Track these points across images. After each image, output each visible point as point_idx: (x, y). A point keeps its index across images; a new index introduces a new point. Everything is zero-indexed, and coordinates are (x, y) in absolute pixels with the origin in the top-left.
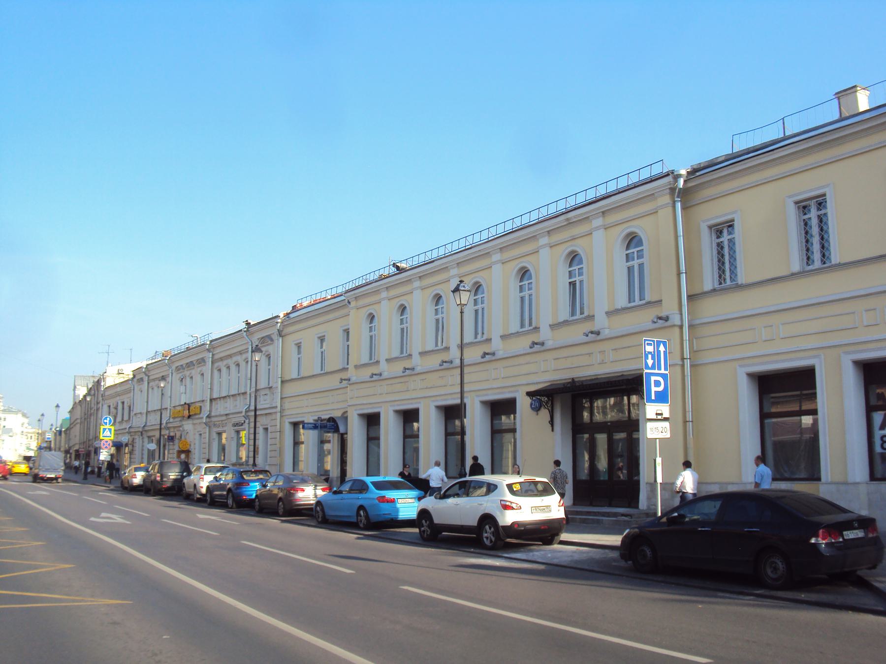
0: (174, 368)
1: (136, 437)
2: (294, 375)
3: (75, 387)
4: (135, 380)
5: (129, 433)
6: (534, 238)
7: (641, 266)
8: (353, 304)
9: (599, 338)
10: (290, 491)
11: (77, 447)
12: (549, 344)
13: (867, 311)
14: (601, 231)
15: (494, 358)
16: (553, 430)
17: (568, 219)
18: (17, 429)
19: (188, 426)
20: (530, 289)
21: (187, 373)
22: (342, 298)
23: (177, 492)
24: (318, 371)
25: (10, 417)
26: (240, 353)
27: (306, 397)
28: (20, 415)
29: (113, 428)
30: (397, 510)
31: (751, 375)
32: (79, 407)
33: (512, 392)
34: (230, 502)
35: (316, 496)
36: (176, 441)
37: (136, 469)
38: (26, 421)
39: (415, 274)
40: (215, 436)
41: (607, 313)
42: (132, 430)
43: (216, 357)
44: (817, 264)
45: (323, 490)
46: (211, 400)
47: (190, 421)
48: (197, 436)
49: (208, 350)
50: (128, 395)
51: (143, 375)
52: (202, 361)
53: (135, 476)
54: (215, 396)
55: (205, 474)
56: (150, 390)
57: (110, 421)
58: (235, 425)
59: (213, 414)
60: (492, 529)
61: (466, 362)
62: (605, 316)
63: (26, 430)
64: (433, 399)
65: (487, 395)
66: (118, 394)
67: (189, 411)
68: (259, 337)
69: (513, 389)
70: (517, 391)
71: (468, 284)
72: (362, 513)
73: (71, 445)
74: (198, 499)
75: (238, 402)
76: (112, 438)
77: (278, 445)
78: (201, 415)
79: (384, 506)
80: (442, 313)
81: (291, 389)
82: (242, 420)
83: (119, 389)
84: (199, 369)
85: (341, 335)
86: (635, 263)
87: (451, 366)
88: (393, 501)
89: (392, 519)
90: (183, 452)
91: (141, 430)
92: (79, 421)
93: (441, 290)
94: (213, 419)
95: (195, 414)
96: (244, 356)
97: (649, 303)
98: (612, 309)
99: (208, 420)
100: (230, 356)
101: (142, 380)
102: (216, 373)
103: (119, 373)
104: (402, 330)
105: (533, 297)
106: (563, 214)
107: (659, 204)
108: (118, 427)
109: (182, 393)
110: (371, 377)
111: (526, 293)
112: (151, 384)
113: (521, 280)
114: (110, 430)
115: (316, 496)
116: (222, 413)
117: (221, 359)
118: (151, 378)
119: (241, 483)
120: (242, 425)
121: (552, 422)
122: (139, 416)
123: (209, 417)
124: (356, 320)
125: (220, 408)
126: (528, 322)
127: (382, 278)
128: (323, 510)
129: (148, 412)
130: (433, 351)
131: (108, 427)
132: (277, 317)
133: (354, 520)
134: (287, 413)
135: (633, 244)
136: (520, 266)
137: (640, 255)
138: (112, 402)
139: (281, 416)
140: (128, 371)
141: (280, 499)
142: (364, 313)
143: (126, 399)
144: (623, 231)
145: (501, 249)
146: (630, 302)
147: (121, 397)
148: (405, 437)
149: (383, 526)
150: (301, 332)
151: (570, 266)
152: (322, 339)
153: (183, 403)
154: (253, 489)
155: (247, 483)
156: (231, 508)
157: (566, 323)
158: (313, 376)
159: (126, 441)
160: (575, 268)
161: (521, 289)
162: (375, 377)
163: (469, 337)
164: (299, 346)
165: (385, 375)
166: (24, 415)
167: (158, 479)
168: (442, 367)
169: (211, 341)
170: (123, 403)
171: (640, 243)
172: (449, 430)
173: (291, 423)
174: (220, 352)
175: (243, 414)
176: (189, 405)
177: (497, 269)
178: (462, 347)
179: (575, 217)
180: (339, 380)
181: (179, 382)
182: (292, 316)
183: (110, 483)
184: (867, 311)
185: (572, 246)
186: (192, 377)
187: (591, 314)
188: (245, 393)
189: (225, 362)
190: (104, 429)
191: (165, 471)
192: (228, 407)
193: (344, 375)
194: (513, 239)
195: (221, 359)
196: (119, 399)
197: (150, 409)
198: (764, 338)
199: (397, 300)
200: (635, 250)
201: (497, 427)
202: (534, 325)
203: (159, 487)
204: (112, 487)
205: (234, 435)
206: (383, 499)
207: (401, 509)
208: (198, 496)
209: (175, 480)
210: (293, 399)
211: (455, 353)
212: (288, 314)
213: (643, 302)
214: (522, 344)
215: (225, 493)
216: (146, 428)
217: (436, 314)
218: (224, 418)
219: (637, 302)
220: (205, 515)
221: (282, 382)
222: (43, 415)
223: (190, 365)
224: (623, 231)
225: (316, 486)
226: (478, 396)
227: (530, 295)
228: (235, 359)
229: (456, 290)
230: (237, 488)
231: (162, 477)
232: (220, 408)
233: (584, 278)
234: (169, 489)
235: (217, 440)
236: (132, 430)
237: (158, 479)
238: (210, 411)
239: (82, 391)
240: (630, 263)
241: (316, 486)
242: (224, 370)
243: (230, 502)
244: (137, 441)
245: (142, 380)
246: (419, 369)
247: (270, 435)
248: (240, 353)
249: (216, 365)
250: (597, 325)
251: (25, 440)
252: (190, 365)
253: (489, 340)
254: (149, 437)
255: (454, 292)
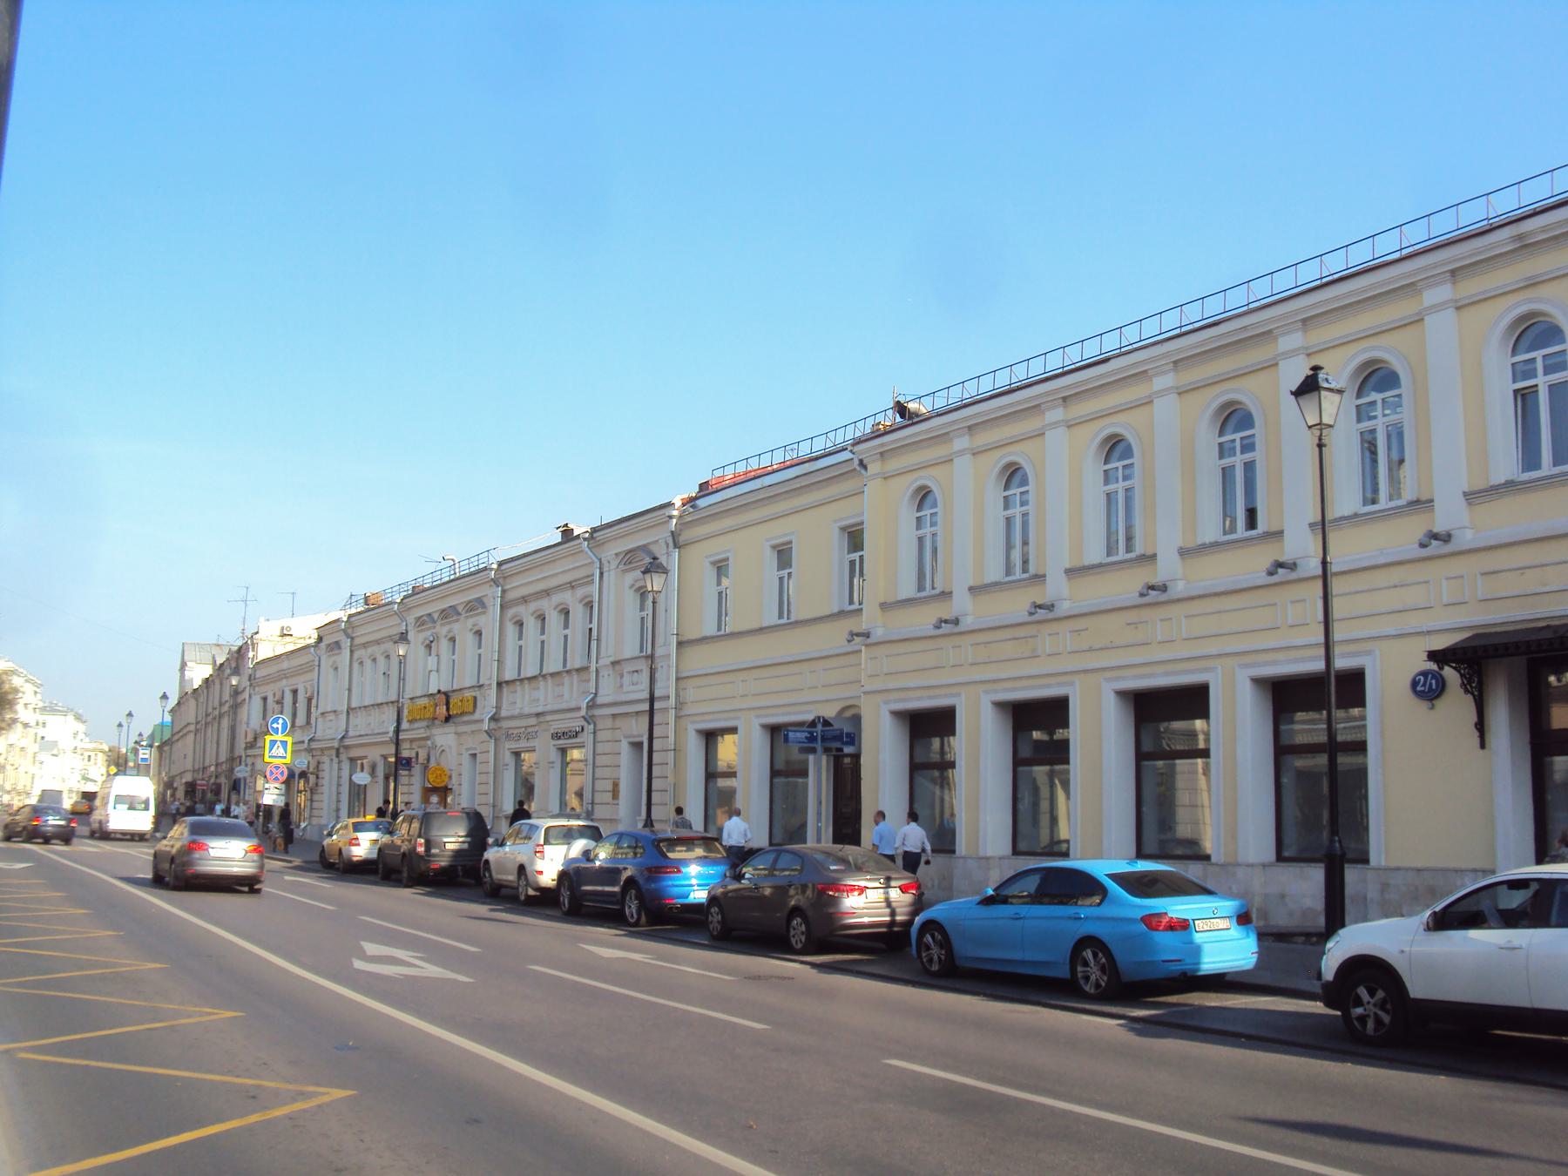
0: (411, 619)
1: (326, 759)
2: (710, 629)
3: (183, 665)
4: (323, 645)
5: (309, 750)
6: (1035, 409)
7: (1249, 467)
8: (874, 468)
9: (1293, 576)
10: (826, 895)
11: (188, 778)
12: (1179, 588)
13: (1293, 602)
14: (1062, 430)
15: (1051, 616)
16: (1483, 746)
17: (1520, 237)
18: (66, 743)
19: (445, 737)
20: (933, 524)
21: (443, 631)
22: (846, 455)
23: (466, 877)
24: (772, 618)
25: (51, 720)
26: (572, 586)
27: (805, 667)
28: (71, 718)
29: (289, 740)
30: (1197, 951)
31: (1258, 682)
32: (192, 703)
33: (1060, 684)
34: (632, 908)
35: (888, 903)
36: (417, 769)
37: (358, 827)
38: (81, 728)
39: (1048, 393)
40: (509, 759)
41: (1465, 494)
42: (314, 745)
43: (511, 596)
44: (1018, 574)
45: (904, 889)
46: (499, 684)
47: (450, 728)
48: (466, 760)
49: (495, 582)
50: (308, 676)
51: (341, 637)
52: (477, 606)
53: (354, 842)
54: (509, 674)
55: (547, 842)
56: (356, 665)
57: (285, 724)
58: (556, 736)
59: (504, 713)
60: (1380, 994)
61: (1334, 568)
62: (1177, 557)
63: (80, 745)
64: (1108, 674)
65: (1274, 663)
66: (283, 675)
67: (449, 708)
68: (639, 547)
69: (732, 715)
70: (958, 695)
71: (1339, 370)
72: (1088, 954)
73: (173, 773)
74: (528, 897)
75: (566, 689)
76: (288, 760)
77: (671, 780)
78: (477, 716)
79: (1163, 938)
80: (933, 524)
81: (699, 660)
82: (576, 724)
83: (285, 665)
84: (470, 622)
85: (835, 542)
86: (1238, 460)
87: (956, 630)
88: (1183, 925)
89: (1184, 974)
90: (434, 790)
91: (336, 745)
92: (192, 728)
93: (1247, 392)
94: (504, 724)
95: (463, 714)
96: (580, 592)
97: (797, 622)
98: (1480, 484)
99: (493, 725)
100: (547, 593)
101: (337, 645)
102: (511, 630)
103: (283, 635)
104: (720, 593)
105: (1031, 519)
106: (939, 415)
107: (1426, 304)
108: (299, 736)
109: (429, 674)
110: (938, 627)
111: (1017, 511)
112: (357, 654)
113: (920, 508)
114: (284, 743)
115: (888, 903)
116: (527, 710)
117: (525, 600)
118: (357, 641)
119: (660, 867)
120: (576, 735)
121: (1481, 726)
122: (332, 717)
123: (494, 719)
124: (882, 504)
125: (521, 702)
126: (1125, 546)
127: (877, 434)
128: (946, 943)
129: (350, 710)
130: (1100, 565)
131: (279, 737)
132: (670, 505)
133: (1063, 972)
134: (688, 710)
135: (1116, 453)
136: (918, 483)
137: (1248, 446)
138: (270, 691)
139: (677, 717)
140: (305, 630)
141: (796, 911)
142: (905, 487)
143: (301, 683)
144: (1217, 396)
145: (1304, 321)
146: (1109, 554)
147: (293, 681)
148: (916, 768)
149: (1152, 990)
150: (1387, 335)
151: (1007, 487)
152: (784, 555)
153: (433, 690)
154: (695, 881)
155: (676, 867)
156: (636, 924)
157: (1510, 486)
158: (761, 630)
159: (304, 767)
160: (1015, 491)
161: (1007, 503)
162: (946, 628)
163: (1346, 500)
164: (721, 568)
165: (968, 622)
166: (79, 718)
167: (421, 849)
168: (1425, 552)
169: (501, 564)
170: (295, 692)
171: (1128, 452)
172: (919, 759)
173: (699, 732)
174: (520, 586)
175: (583, 712)
176: (446, 694)
177: (963, 465)
178: (1322, 527)
179: (1544, 229)
180: (846, 636)
181: (422, 650)
182: (702, 503)
183: (286, 851)
184: (1293, 602)
185: (1530, 301)
186: (453, 640)
187: (1149, 552)
188: (586, 669)
189: (533, 606)
190: (273, 743)
191: (435, 833)
192: (543, 697)
193: (851, 624)
194: (1313, 306)
195: (525, 600)
196: (286, 686)
197: (354, 705)
198: (1290, 622)
199: (998, 454)
200: (1120, 464)
201: (1285, 741)
202: (1032, 570)
203: (423, 867)
204: (297, 862)
205: (554, 756)
206: (1152, 921)
207: (1206, 948)
208: (531, 892)
209: (458, 854)
210: (705, 681)
211: (1301, 545)
212: (691, 501)
213: (1132, 555)
214: (922, 620)
215: (616, 889)
216: (347, 742)
217: (919, 527)
218: (533, 721)
219: (1121, 555)
220: (693, 964)
221: (680, 644)
222: (130, 715)
223: (449, 614)
224: (1217, 396)
225: (888, 879)
226: (1109, 680)
227: (1025, 515)
228: (556, 599)
229: (1309, 386)
230: (649, 879)
231: (428, 845)
232: (521, 702)
233: (1029, 508)
234: (443, 872)
235: (512, 764)
236: (314, 745)
237: (421, 849)
238: (498, 708)
239: (199, 673)
240: (1227, 461)
241: (888, 879)
242: (531, 625)
243: (632, 908)
244: (326, 766)
245: (337, 645)
246: (1064, 607)
247: (479, 768)
248: (572, 586)
249: (511, 612)
250: (863, 624)
251: (79, 763)
252: (449, 614)
253: (946, 595)
254: (352, 760)
255: (1299, 393)
